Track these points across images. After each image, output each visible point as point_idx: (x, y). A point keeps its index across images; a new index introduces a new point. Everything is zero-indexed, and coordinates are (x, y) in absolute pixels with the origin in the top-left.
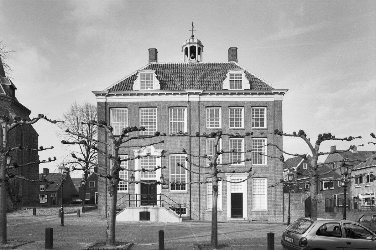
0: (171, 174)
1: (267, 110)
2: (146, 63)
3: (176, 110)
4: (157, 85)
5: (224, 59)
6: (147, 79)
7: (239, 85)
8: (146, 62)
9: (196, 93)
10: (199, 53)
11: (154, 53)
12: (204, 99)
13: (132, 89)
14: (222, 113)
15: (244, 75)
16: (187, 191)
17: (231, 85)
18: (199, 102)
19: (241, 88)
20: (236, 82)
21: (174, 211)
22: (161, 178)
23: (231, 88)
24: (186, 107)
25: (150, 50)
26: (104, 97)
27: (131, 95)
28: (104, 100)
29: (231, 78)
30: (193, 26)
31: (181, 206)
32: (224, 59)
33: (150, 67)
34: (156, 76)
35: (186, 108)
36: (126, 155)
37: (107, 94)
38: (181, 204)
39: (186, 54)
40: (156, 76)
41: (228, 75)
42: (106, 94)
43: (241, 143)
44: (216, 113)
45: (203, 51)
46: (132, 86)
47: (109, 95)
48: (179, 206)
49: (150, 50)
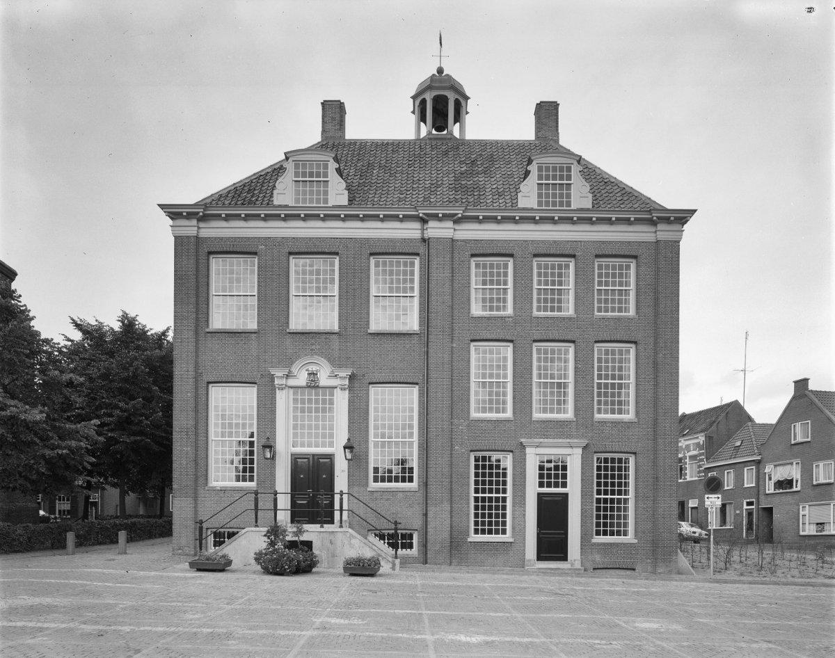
0: (374, 438)
1: (638, 266)
2: (316, 137)
3: (614, 268)
4: (337, 194)
5: (525, 130)
6: (383, 436)
7: (561, 196)
8: (311, 133)
9: (446, 217)
10: (457, 118)
11: (334, 112)
12: (469, 232)
13: (270, 204)
14: (575, 357)
15: (575, 169)
16: (417, 486)
17: (540, 195)
18: (453, 240)
19: (569, 204)
20: (554, 189)
21: (382, 542)
22: (345, 448)
23: (540, 203)
24: (418, 254)
25: (325, 104)
26: (194, 222)
27: (267, 218)
28: (192, 231)
29: (540, 177)
30: (441, 45)
31: (399, 526)
32: (525, 130)
33: (322, 147)
34: (336, 169)
35: (418, 258)
36: (253, 383)
37: (201, 214)
38: (399, 521)
39: (423, 118)
40: (336, 169)
41: (533, 168)
42: (198, 213)
43: (567, 356)
44: (499, 274)
45: (467, 113)
46: (271, 196)
47: (204, 218)
48: (393, 526)
49: (325, 104)
